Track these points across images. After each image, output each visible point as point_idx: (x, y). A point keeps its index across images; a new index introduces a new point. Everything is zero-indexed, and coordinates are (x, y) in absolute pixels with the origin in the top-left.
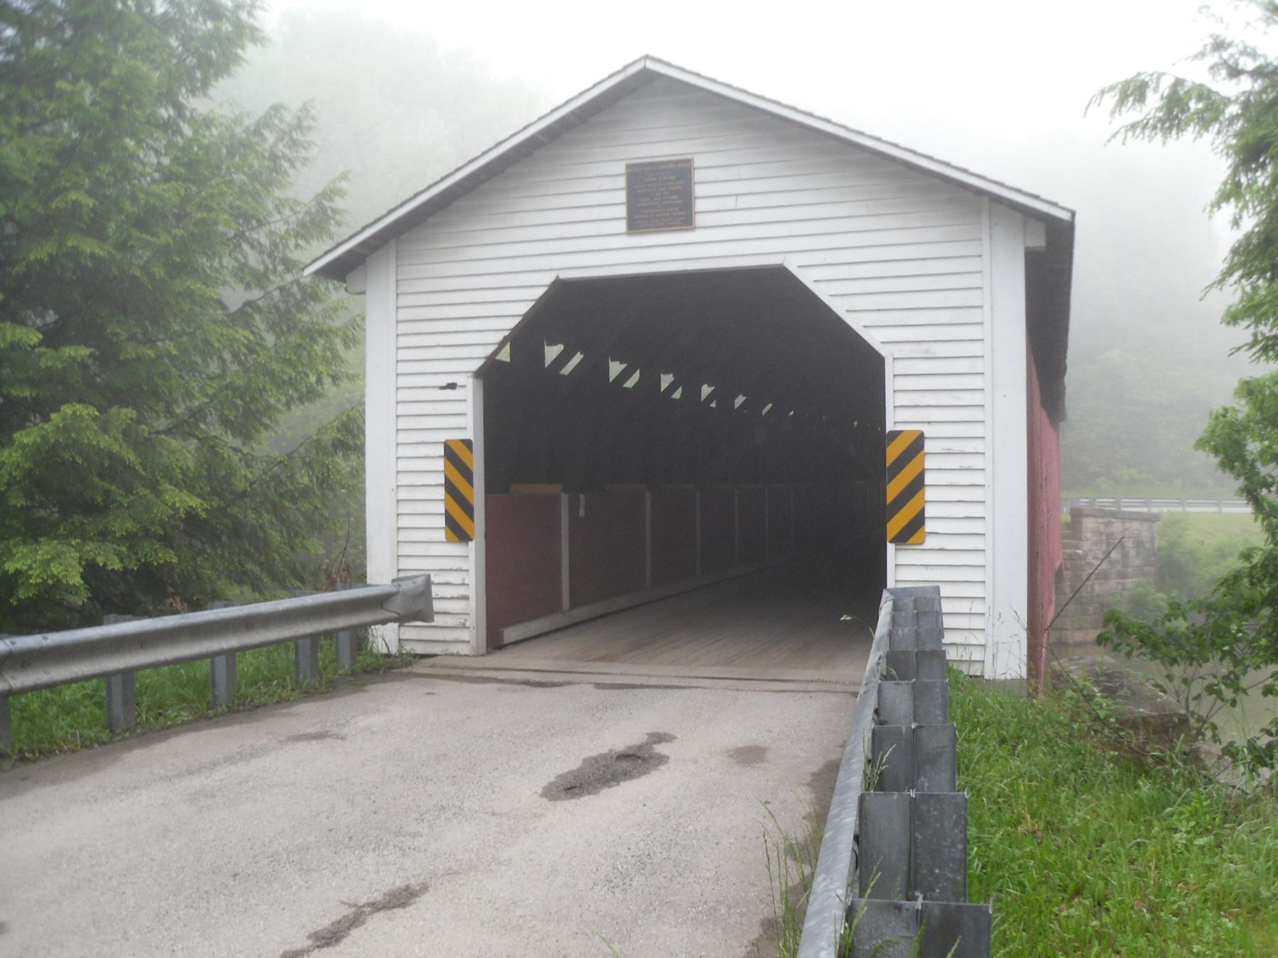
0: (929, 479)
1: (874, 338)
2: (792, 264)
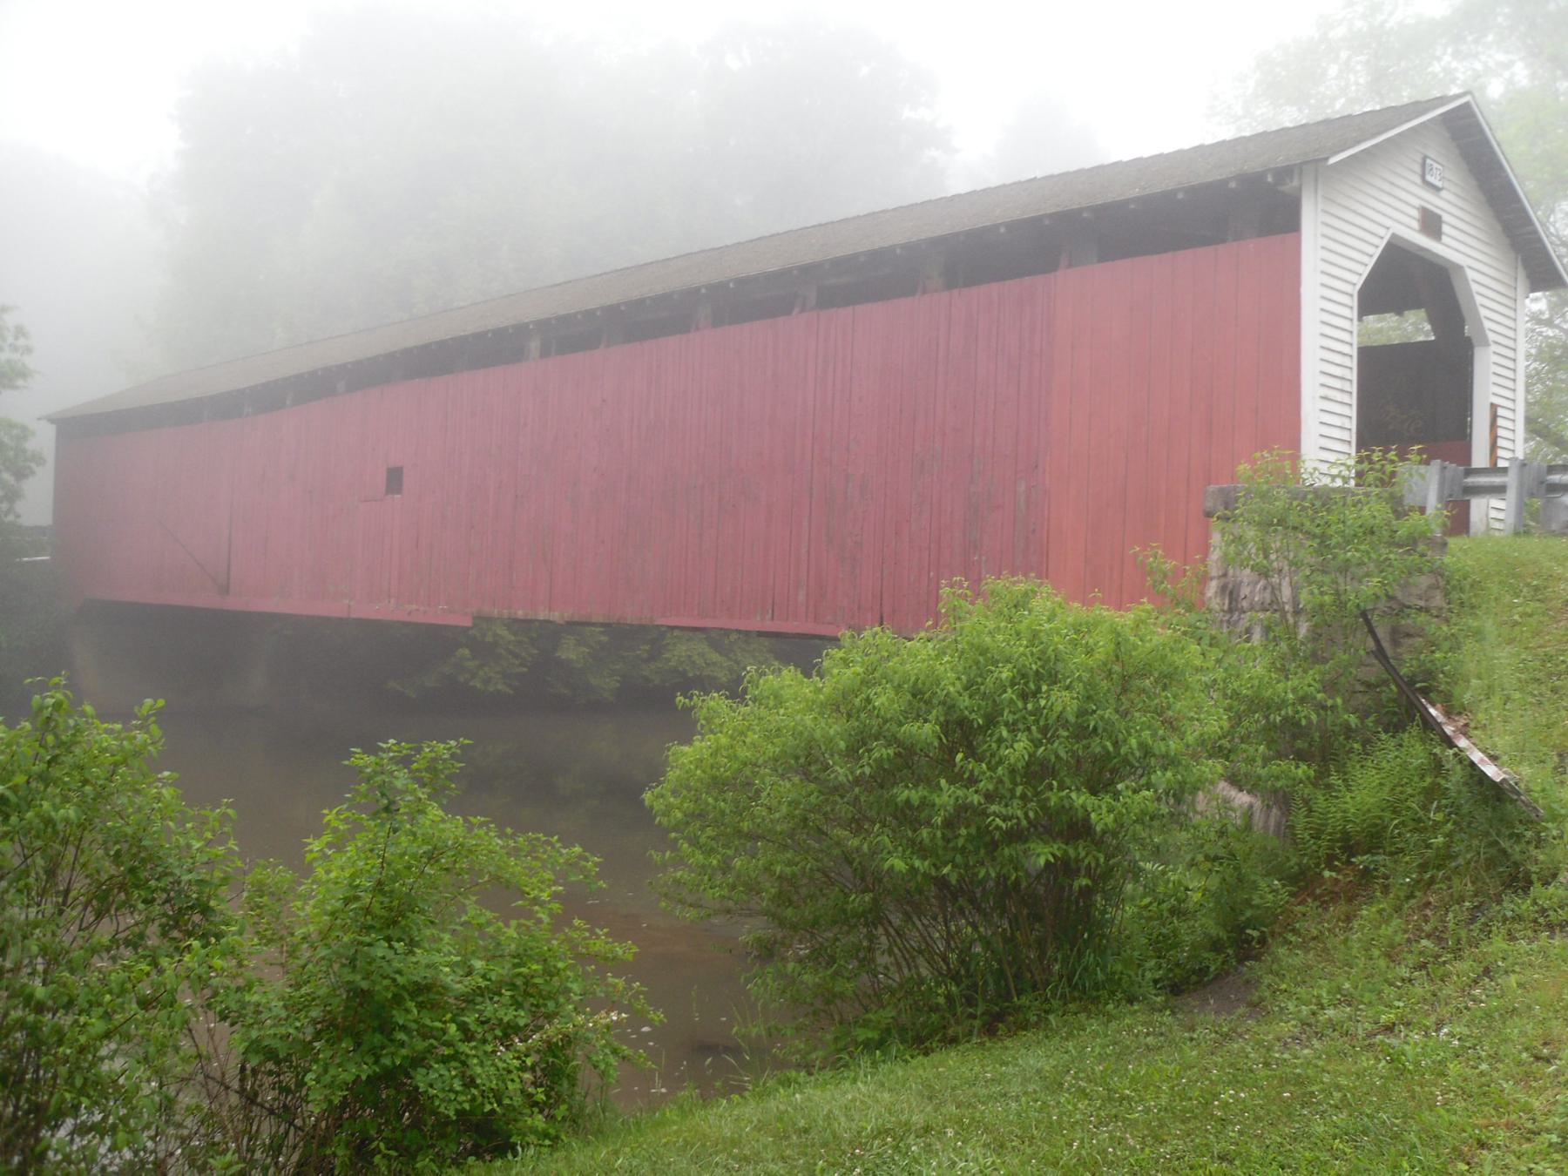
1: (1491, 337)
2: (1471, 274)
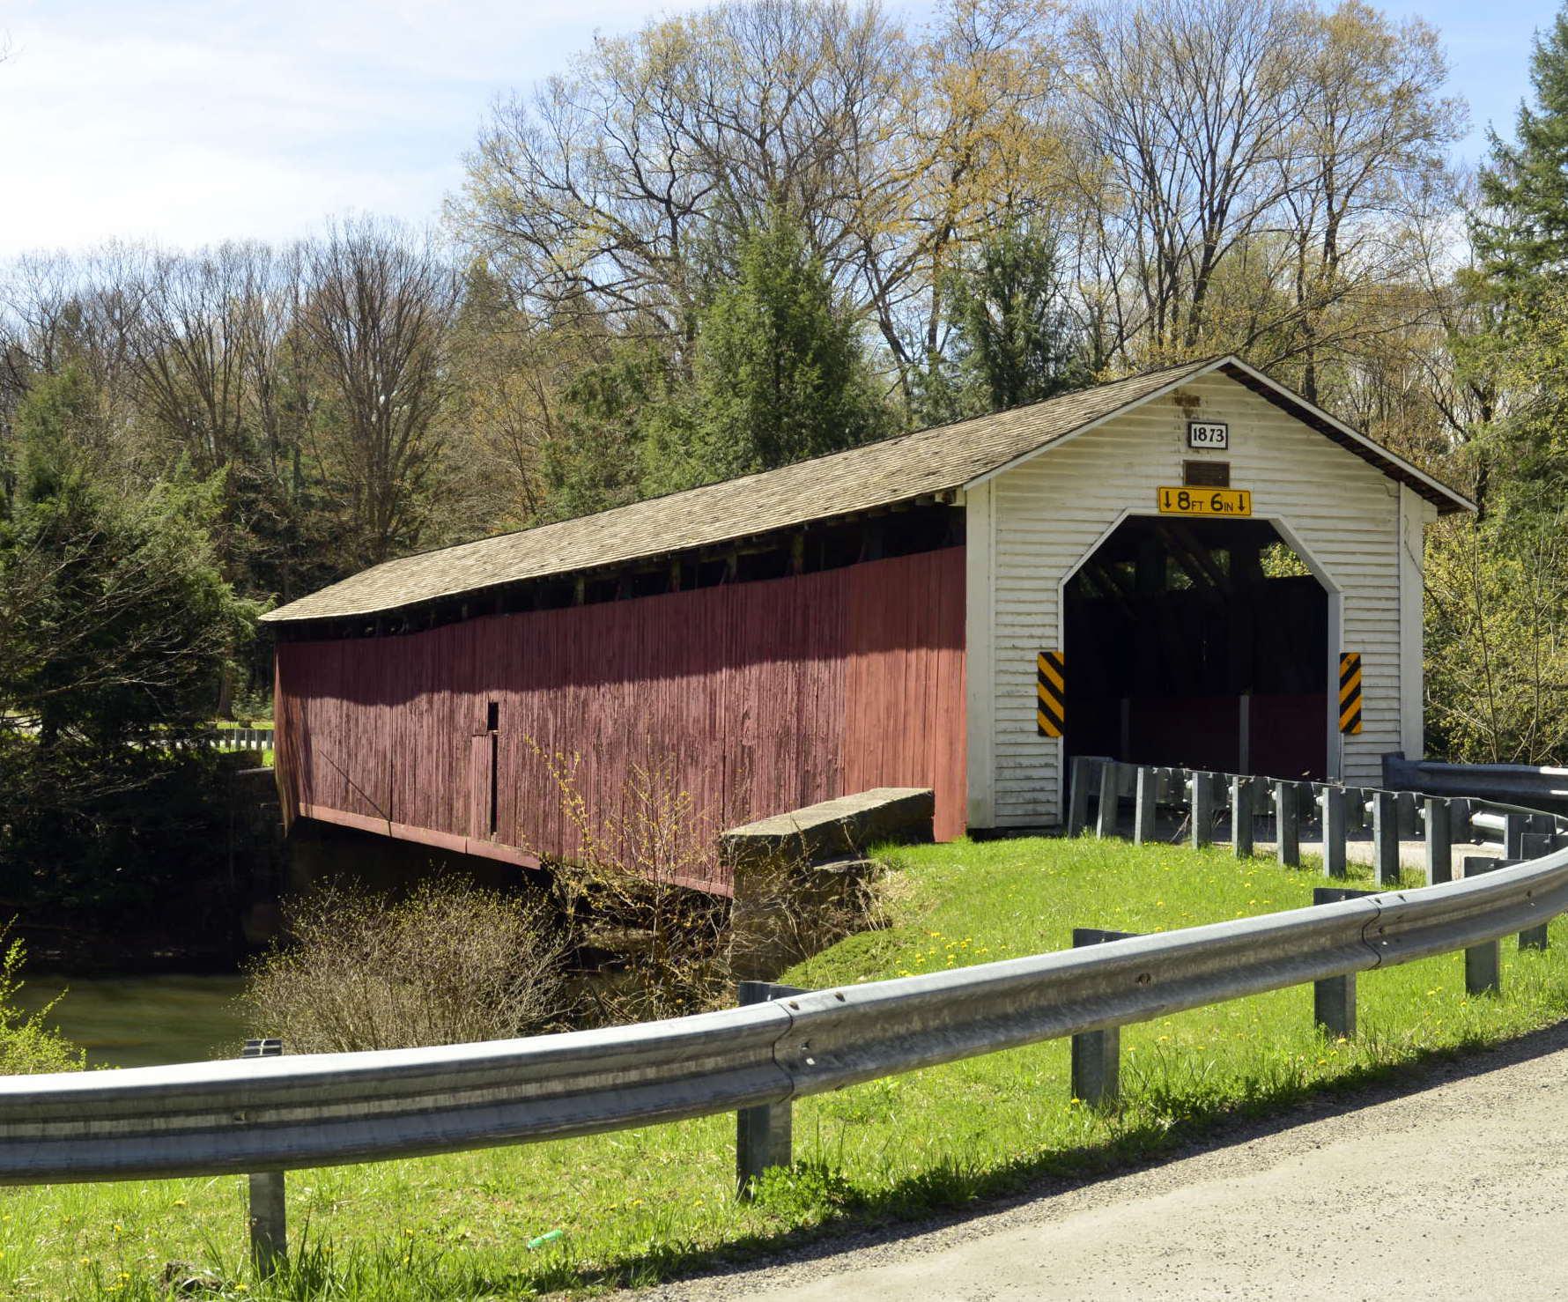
0: (1363, 716)
1: (1336, 583)
